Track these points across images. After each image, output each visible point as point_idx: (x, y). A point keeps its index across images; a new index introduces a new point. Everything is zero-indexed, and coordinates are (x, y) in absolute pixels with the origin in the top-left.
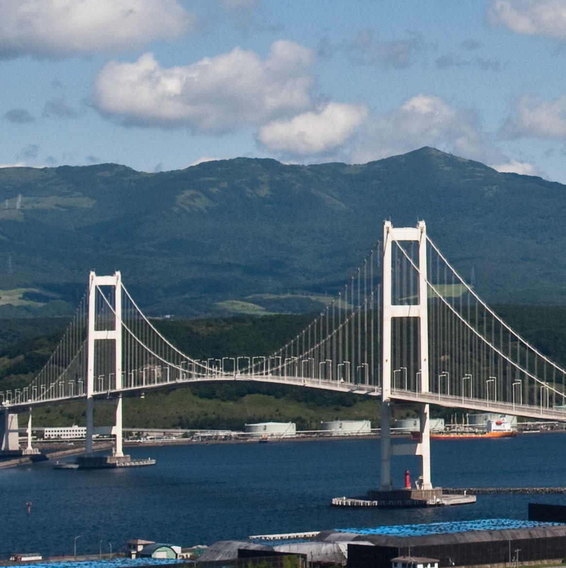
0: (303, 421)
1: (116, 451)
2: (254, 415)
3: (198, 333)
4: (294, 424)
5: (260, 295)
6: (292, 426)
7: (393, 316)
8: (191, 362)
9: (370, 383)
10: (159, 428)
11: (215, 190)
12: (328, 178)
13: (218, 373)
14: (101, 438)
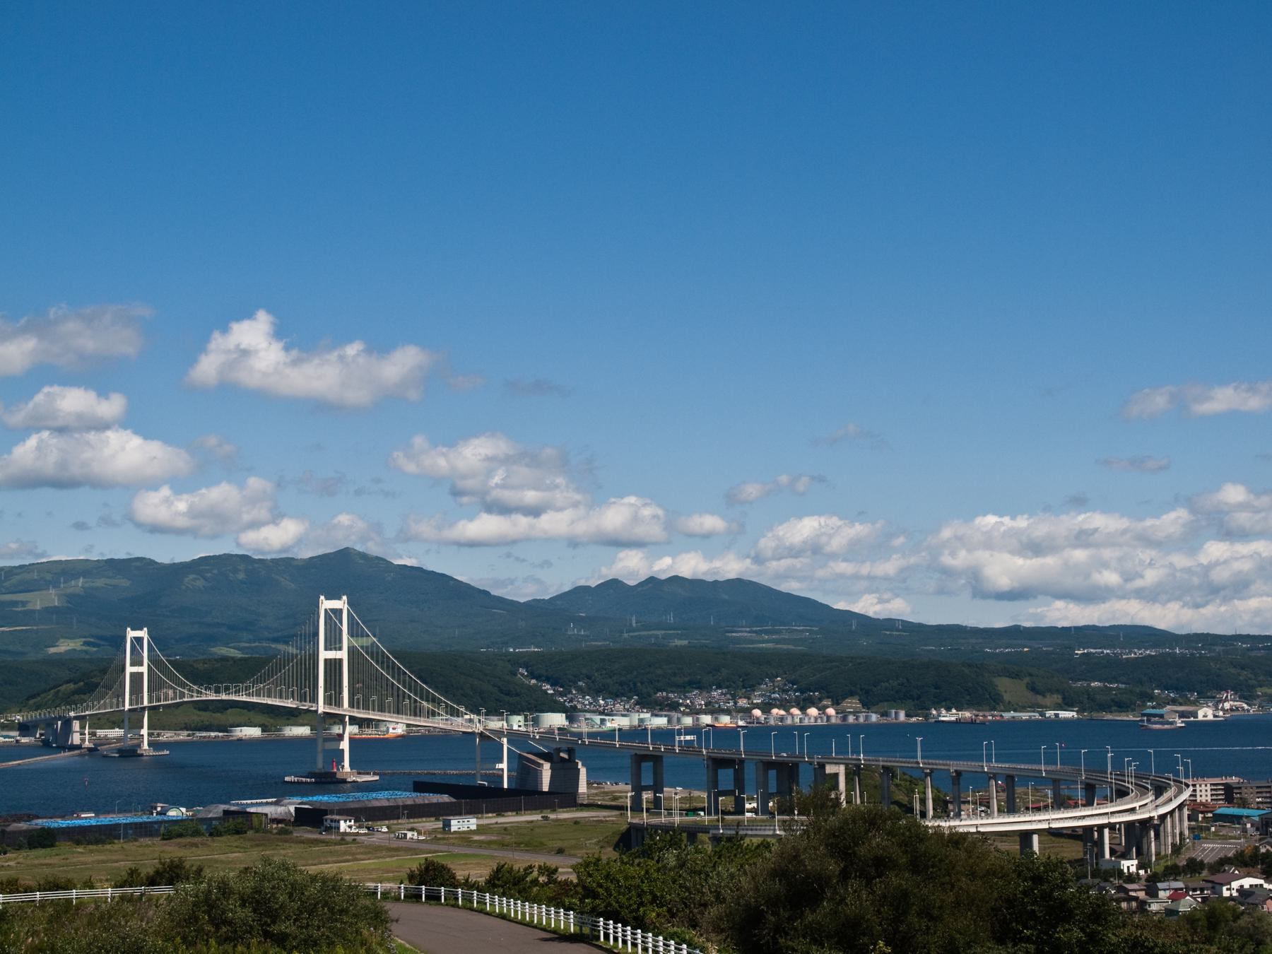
0: (266, 726)
3: (197, 669)
9: (310, 702)
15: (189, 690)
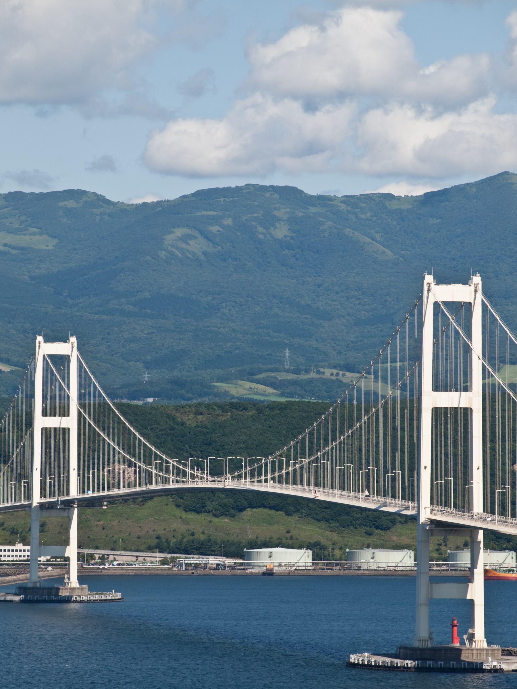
0: (323, 548)
1: (69, 579)
2: (257, 538)
3: (183, 424)
4: (310, 552)
5: (273, 374)
6: (306, 554)
7: (434, 406)
8: (167, 462)
9: (404, 498)
10: (131, 550)
11: (215, 229)
12: (369, 215)
13: (202, 478)
14: (53, 561)
15: (160, 468)
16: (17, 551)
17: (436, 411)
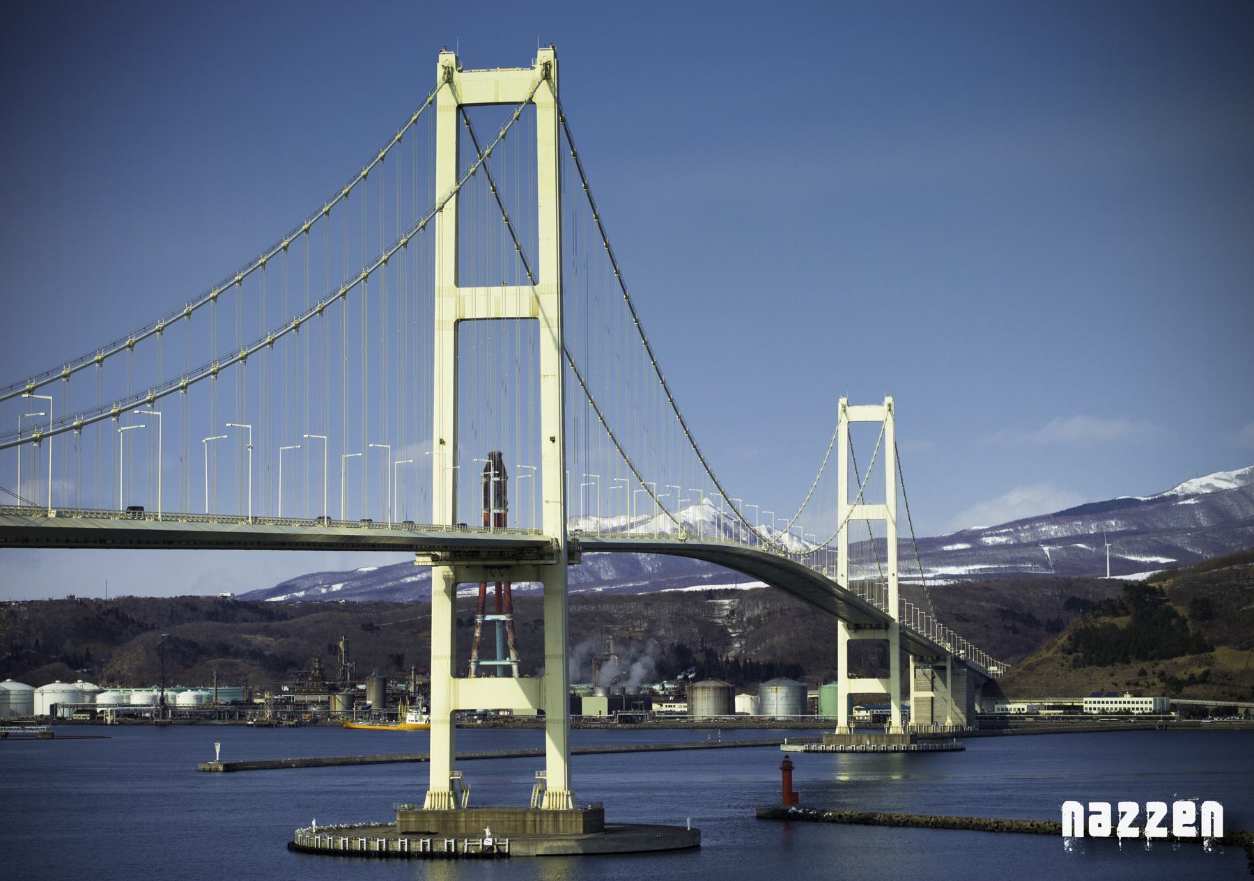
16: (1125, 702)
17: (882, 500)
